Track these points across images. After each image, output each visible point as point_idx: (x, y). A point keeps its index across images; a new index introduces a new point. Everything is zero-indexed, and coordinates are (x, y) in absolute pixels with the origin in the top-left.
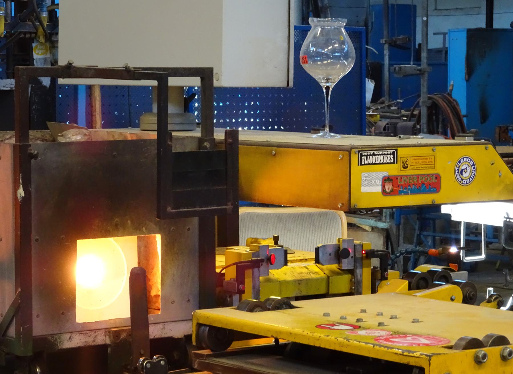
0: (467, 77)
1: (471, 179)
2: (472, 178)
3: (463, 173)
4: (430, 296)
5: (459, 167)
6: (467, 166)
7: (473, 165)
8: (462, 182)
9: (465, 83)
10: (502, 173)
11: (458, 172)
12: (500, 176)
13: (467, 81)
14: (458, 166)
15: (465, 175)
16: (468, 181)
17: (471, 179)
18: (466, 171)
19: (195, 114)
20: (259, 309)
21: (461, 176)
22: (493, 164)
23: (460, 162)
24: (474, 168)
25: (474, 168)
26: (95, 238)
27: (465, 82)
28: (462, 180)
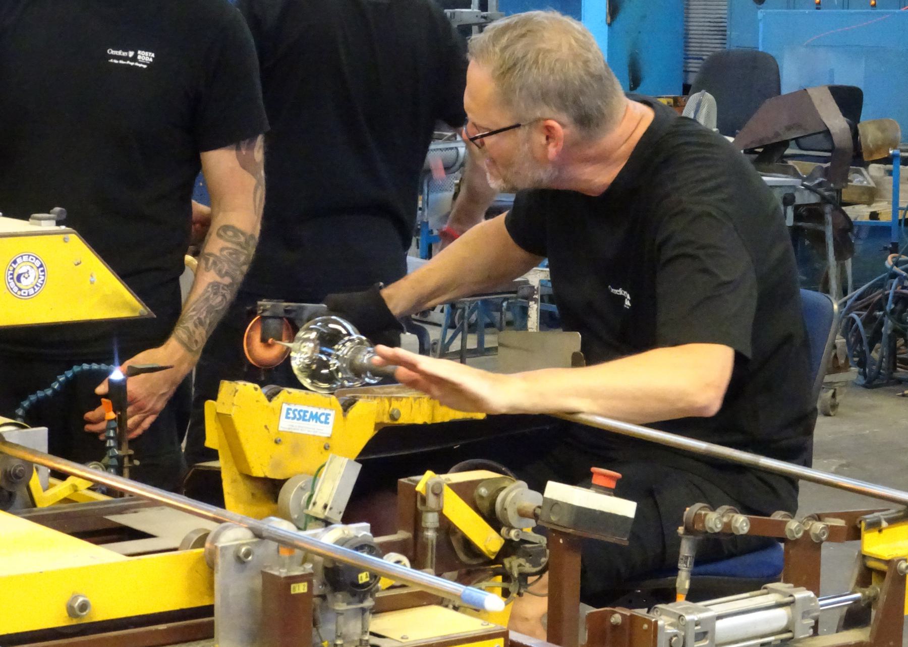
0: (609, 19)
1: (37, 289)
2: (38, 287)
3: (22, 279)
4: (109, 549)
5: (14, 269)
6: (29, 268)
7: (41, 266)
8: (19, 293)
9: (606, 28)
10: (95, 277)
11: (12, 278)
12: (92, 283)
13: (610, 25)
14: (11, 269)
15: (25, 283)
16: (32, 291)
17: (37, 289)
18: (26, 275)
19: (117, 55)
20: (65, 631)
21: (18, 284)
22: (78, 264)
23: (15, 262)
24: (43, 271)
25: (43, 271)
26: (8, 327)
27: (606, 27)
28: (20, 290)
